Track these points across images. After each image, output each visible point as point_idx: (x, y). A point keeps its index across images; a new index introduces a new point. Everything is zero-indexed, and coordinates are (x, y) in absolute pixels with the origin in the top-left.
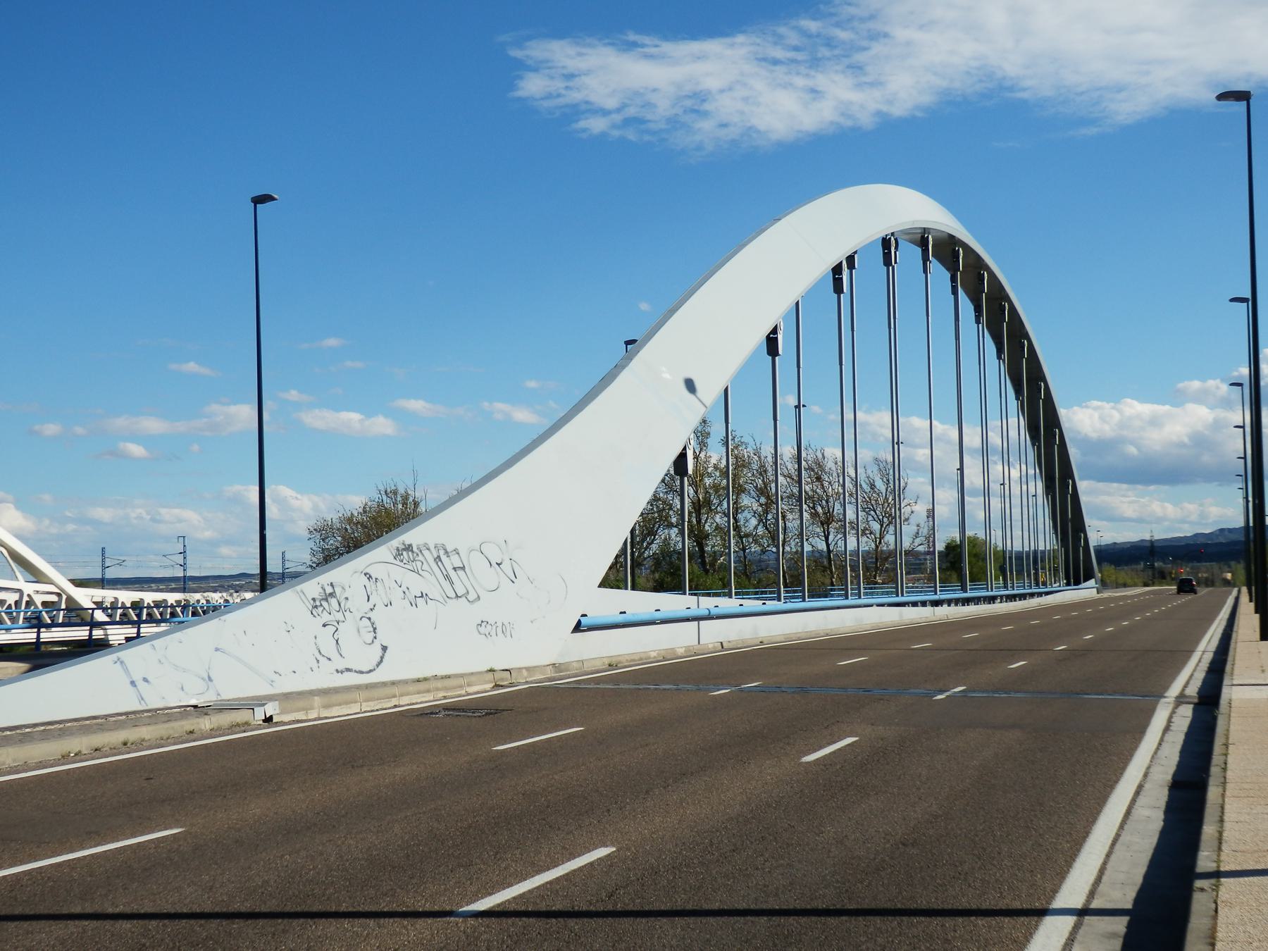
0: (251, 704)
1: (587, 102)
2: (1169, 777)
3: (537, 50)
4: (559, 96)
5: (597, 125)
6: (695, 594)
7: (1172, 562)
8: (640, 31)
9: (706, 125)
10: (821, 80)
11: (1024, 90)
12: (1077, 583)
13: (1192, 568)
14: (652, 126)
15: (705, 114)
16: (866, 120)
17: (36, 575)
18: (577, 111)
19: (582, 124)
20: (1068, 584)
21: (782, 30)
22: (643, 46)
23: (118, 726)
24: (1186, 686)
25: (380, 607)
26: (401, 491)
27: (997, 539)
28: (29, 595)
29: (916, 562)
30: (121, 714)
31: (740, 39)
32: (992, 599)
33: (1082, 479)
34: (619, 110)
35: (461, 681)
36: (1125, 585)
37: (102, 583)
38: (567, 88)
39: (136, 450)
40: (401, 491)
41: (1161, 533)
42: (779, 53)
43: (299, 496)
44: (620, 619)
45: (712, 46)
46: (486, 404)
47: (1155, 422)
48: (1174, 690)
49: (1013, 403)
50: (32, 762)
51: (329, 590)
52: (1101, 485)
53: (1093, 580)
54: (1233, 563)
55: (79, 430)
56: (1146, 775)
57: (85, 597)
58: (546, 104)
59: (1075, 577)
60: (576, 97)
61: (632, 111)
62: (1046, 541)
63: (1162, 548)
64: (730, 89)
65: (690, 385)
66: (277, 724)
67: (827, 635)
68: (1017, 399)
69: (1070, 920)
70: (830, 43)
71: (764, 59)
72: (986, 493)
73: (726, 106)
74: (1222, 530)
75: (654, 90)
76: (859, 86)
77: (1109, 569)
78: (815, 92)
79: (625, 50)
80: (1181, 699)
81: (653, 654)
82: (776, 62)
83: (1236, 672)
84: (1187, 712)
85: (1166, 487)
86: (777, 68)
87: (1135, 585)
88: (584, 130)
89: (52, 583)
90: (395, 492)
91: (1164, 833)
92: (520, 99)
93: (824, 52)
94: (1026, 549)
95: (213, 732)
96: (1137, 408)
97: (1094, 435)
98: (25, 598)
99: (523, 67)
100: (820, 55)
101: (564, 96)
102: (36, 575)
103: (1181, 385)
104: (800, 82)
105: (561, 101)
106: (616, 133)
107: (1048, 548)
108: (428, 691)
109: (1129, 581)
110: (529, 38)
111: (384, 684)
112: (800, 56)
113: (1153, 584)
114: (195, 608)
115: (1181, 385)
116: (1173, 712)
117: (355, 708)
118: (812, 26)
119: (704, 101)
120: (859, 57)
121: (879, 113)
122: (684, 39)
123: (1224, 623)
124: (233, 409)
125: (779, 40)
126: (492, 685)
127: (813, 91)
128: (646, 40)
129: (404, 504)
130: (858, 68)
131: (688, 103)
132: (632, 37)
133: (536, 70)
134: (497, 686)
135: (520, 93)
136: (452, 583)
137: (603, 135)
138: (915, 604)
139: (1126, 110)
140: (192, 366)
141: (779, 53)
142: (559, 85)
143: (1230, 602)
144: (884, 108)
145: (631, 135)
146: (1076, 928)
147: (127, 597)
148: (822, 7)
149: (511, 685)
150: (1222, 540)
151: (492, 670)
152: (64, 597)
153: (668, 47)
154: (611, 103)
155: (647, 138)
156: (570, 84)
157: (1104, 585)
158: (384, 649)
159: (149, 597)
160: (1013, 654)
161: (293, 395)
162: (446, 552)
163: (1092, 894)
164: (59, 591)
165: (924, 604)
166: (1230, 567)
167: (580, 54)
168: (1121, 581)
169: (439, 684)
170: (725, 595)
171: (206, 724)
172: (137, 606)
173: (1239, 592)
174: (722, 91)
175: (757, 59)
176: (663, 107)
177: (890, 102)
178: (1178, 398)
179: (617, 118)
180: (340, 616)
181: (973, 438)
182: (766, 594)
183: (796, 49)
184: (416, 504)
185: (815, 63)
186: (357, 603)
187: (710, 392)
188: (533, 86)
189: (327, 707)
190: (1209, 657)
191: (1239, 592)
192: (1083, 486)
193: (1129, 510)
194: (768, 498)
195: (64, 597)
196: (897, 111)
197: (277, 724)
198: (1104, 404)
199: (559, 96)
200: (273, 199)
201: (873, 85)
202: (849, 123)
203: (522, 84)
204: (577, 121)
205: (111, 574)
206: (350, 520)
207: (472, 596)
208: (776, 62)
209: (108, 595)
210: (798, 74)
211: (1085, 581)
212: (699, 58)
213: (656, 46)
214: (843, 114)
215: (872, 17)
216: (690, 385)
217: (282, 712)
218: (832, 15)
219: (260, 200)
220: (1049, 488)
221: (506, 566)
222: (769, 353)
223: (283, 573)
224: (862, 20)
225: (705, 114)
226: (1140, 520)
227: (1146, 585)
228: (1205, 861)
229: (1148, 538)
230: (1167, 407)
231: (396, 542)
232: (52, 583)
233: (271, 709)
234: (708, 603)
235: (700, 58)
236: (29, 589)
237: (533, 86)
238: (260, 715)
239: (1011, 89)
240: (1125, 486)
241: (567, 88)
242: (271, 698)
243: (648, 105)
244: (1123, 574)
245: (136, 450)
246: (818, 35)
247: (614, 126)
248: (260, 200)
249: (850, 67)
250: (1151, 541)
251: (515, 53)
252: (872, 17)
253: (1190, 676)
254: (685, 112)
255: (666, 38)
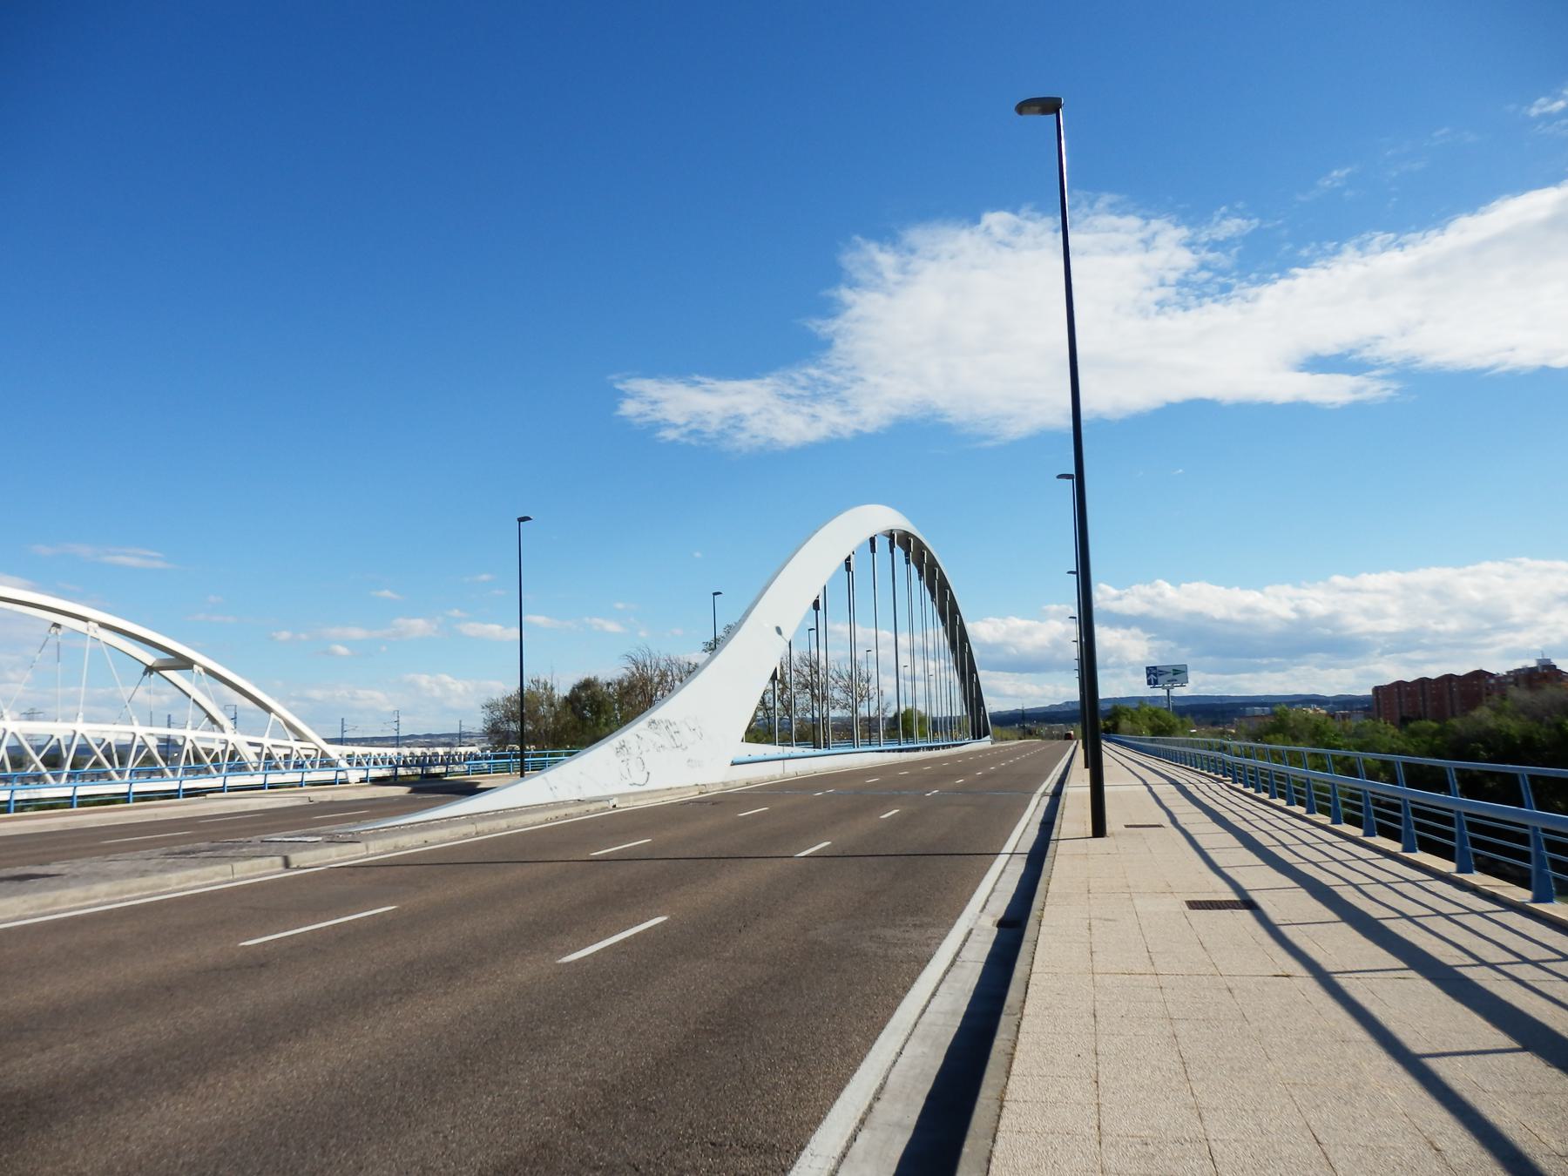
0: (607, 799)
1: (665, 420)
2: (1040, 820)
3: (635, 385)
4: (646, 415)
5: (671, 435)
6: (783, 745)
7: (1037, 724)
8: (701, 374)
9: (743, 436)
10: (818, 409)
11: (949, 416)
12: (980, 738)
13: (1049, 728)
14: (706, 436)
15: (742, 429)
16: (847, 434)
17: (301, 737)
18: (658, 426)
19: (662, 434)
20: (974, 739)
21: (796, 376)
22: (704, 383)
23: (526, 812)
24: (1046, 789)
25: (644, 753)
26: (542, 681)
27: (921, 707)
28: (297, 751)
29: (870, 726)
30: (437, 820)
31: (768, 380)
32: (917, 749)
33: (981, 669)
34: (686, 425)
35: (685, 790)
36: (1007, 739)
37: (341, 741)
38: (652, 410)
39: (342, 650)
40: (542, 681)
41: (1029, 705)
42: (792, 391)
43: (455, 681)
44: (749, 759)
45: (748, 385)
46: (587, 619)
47: (1028, 632)
48: (1041, 790)
49: (941, 629)
50: (537, 821)
51: (623, 744)
52: (992, 673)
53: (989, 737)
54: (1074, 724)
55: (303, 636)
56: (1030, 820)
57: (334, 751)
58: (638, 420)
59: (979, 733)
60: (658, 416)
61: (694, 426)
62: (958, 710)
63: (1030, 714)
64: (759, 413)
65: (779, 630)
66: (620, 808)
67: (748, 784)
68: (943, 625)
69: (1009, 855)
70: (826, 384)
71: (782, 395)
72: (913, 678)
73: (757, 425)
74: (1067, 703)
75: (709, 413)
76: (844, 413)
77: (998, 729)
78: (814, 417)
79: (691, 386)
80: (1044, 794)
81: (766, 778)
82: (789, 397)
83: (1071, 781)
84: (1046, 800)
85: (1033, 675)
86: (790, 401)
87: (1013, 739)
88: (663, 438)
89: (311, 741)
90: (538, 682)
91: (1038, 836)
92: (621, 417)
93: (822, 390)
94: (940, 716)
95: (596, 811)
96: (1018, 623)
97: (990, 640)
98: (294, 753)
99: (623, 395)
100: (818, 392)
101: (649, 415)
102: (301, 737)
103: (1045, 607)
104: (805, 410)
105: (648, 418)
106: (684, 440)
107: (954, 715)
108: (673, 794)
109: (1009, 737)
110: (630, 377)
111: (649, 792)
112: (806, 393)
113: (1025, 739)
114: (391, 759)
115: (1045, 607)
116: (1040, 799)
117: (645, 802)
118: (814, 372)
119: (741, 421)
120: (845, 394)
121: (856, 431)
122: (731, 380)
123: (1067, 761)
124: (413, 622)
125: (793, 381)
126: (697, 793)
127: (813, 416)
128: (706, 380)
129: (545, 689)
130: (843, 401)
131: (731, 422)
132: (697, 378)
133: (632, 397)
134: (701, 793)
135: (621, 413)
136: (674, 740)
137: (675, 441)
138: (889, 751)
139: (1017, 429)
140: (387, 593)
141: (792, 391)
142: (646, 408)
143: (1072, 749)
144: (860, 428)
145: (694, 442)
146: (1009, 859)
147: (359, 750)
148: (823, 361)
149: (707, 793)
150: (1067, 709)
151: (697, 785)
152: (320, 752)
153: (720, 385)
154: (681, 421)
155: (703, 443)
156: (655, 407)
157: (995, 740)
158: (648, 773)
159: (374, 751)
160: (884, 802)
161: (456, 612)
162: (671, 724)
163: (1014, 850)
164: (316, 748)
165: (894, 751)
166: (1072, 726)
167: (662, 388)
168: (1004, 736)
169: (677, 791)
170: (788, 746)
171: (592, 807)
172: (424, 755)
173: (1078, 743)
174: (754, 415)
175: (779, 395)
176: (715, 424)
177: (864, 423)
178: (1042, 616)
179: (684, 430)
180: (627, 757)
181: (904, 640)
182: (545, 757)
183: (804, 388)
184: (552, 689)
185: (816, 397)
186: (635, 750)
187: (788, 633)
188: (629, 408)
189: (635, 801)
190: (1058, 777)
191: (1078, 743)
192: (981, 673)
193: (1010, 690)
194: (784, 684)
195: (320, 752)
196: (868, 429)
197: (620, 808)
198: (996, 620)
199: (646, 415)
200: (530, 519)
201: (855, 412)
202: (836, 436)
203: (621, 406)
204: (659, 431)
205: (347, 735)
206: (509, 699)
207: (684, 747)
208: (789, 397)
209: (348, 749)
210: (804, 405)
211: (984, 736)
212: (740, 393)
213: (712, 384)
214: (833, 432)
215: (854, 368)
216: (779, 630)
217: (620, 803)
218: (828, 365)
219: (521, 520)
220: (963, 679)
221: (698, 731)
222: (814, 608)
223: (460, 734)
224: (848, 369)
225: (742, 429)
226: (1016, 697)
227: (1021, 739)
228: (1054, 836)
229: (1020, 708)
230: (1037, 622)
231: (648, 719)
232: (311, 741)
233: (615, 801)
234: (788, 751)
235: (739, 392)
236: (297, 746)
237: (629, 408)
238: (611, 804)
239: (941, 416)
240: (1007, 674)
241: (652, 410)
242: (615, 796)
243: (703, 422)
244: (1006, 732)
245: (342, 650)
246: (819, 379)
247: (683, 436)
248: (521, 520)
249: (838, 400)
250: (1023, 711)
251: (619, 386)
252: (854, 368)
253: (1049, 784)
254: (729, 427)
255: (719, 379)
